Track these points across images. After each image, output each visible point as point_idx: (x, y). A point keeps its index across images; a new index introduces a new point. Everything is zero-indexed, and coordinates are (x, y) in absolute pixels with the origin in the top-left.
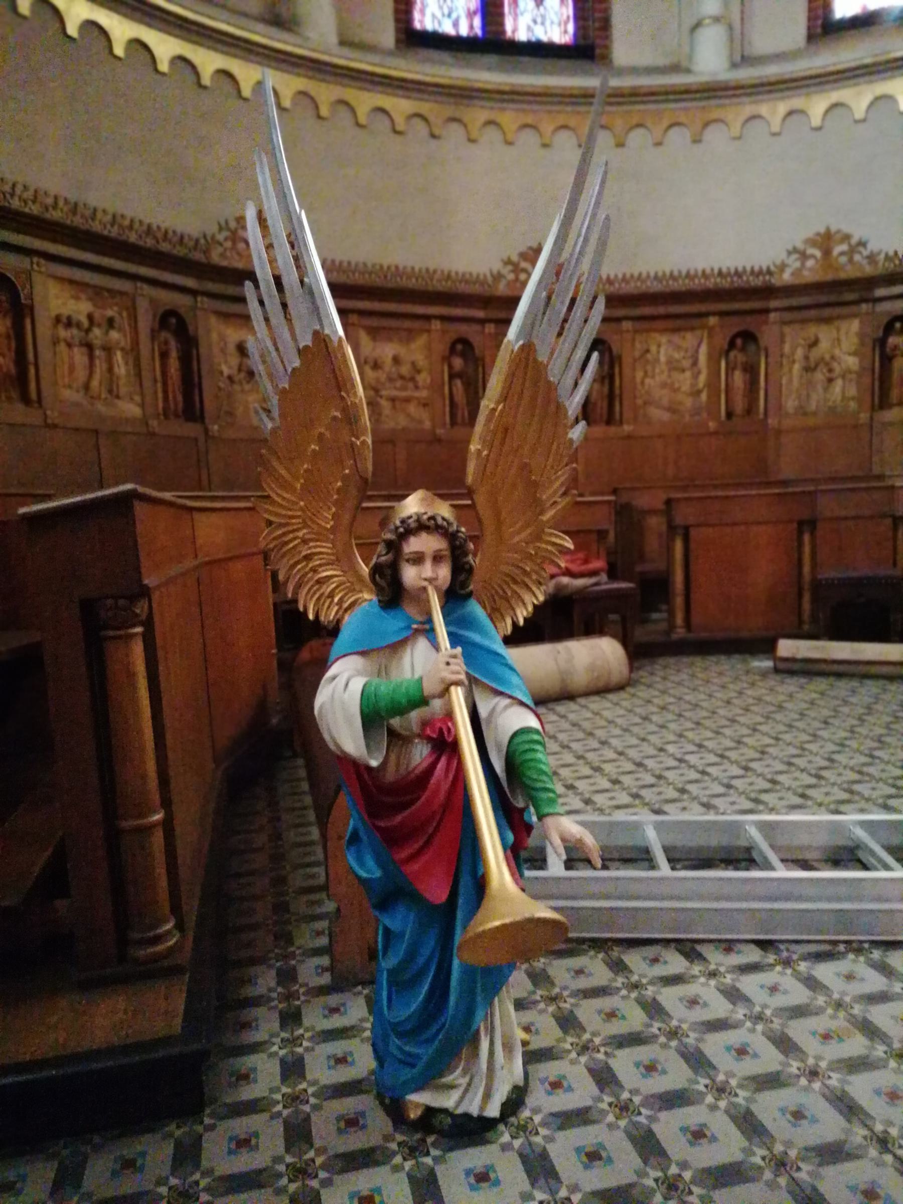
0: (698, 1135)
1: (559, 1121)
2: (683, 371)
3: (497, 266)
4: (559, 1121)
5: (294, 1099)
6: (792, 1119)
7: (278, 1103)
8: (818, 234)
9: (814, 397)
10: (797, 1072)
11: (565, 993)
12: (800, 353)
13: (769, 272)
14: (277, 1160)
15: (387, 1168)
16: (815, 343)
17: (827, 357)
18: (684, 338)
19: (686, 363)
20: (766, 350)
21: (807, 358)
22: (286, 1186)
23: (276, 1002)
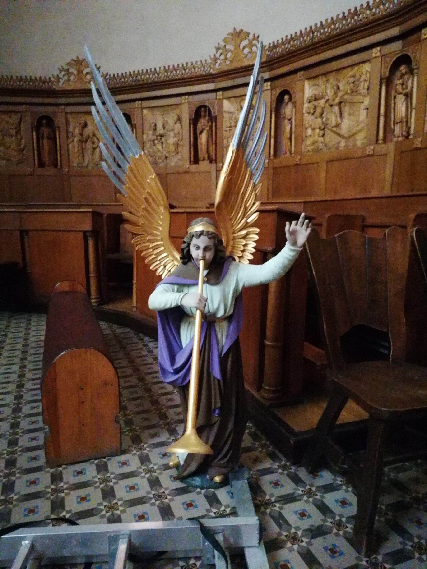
0: (303, 515)
1: (144, 500)
2: (12, 136)
3: (56, 72)
4: (144, 500)
5: (105, 481)
6: (305, 513)
7: (97, 482)
8: (73, 60)
9: (87, 158)
10: (301, 493)
11: (260, 449)
12: (77, 131)
13: (50, 81)
14: (100, 504)
15: (73, 512)
16: (86, 125)
17: (91, 135)
18: (11, 117)
19: (13, 132)
20: (59, 127)
21: (81, 134)
22: (105, 515)
23: (8, 436)
